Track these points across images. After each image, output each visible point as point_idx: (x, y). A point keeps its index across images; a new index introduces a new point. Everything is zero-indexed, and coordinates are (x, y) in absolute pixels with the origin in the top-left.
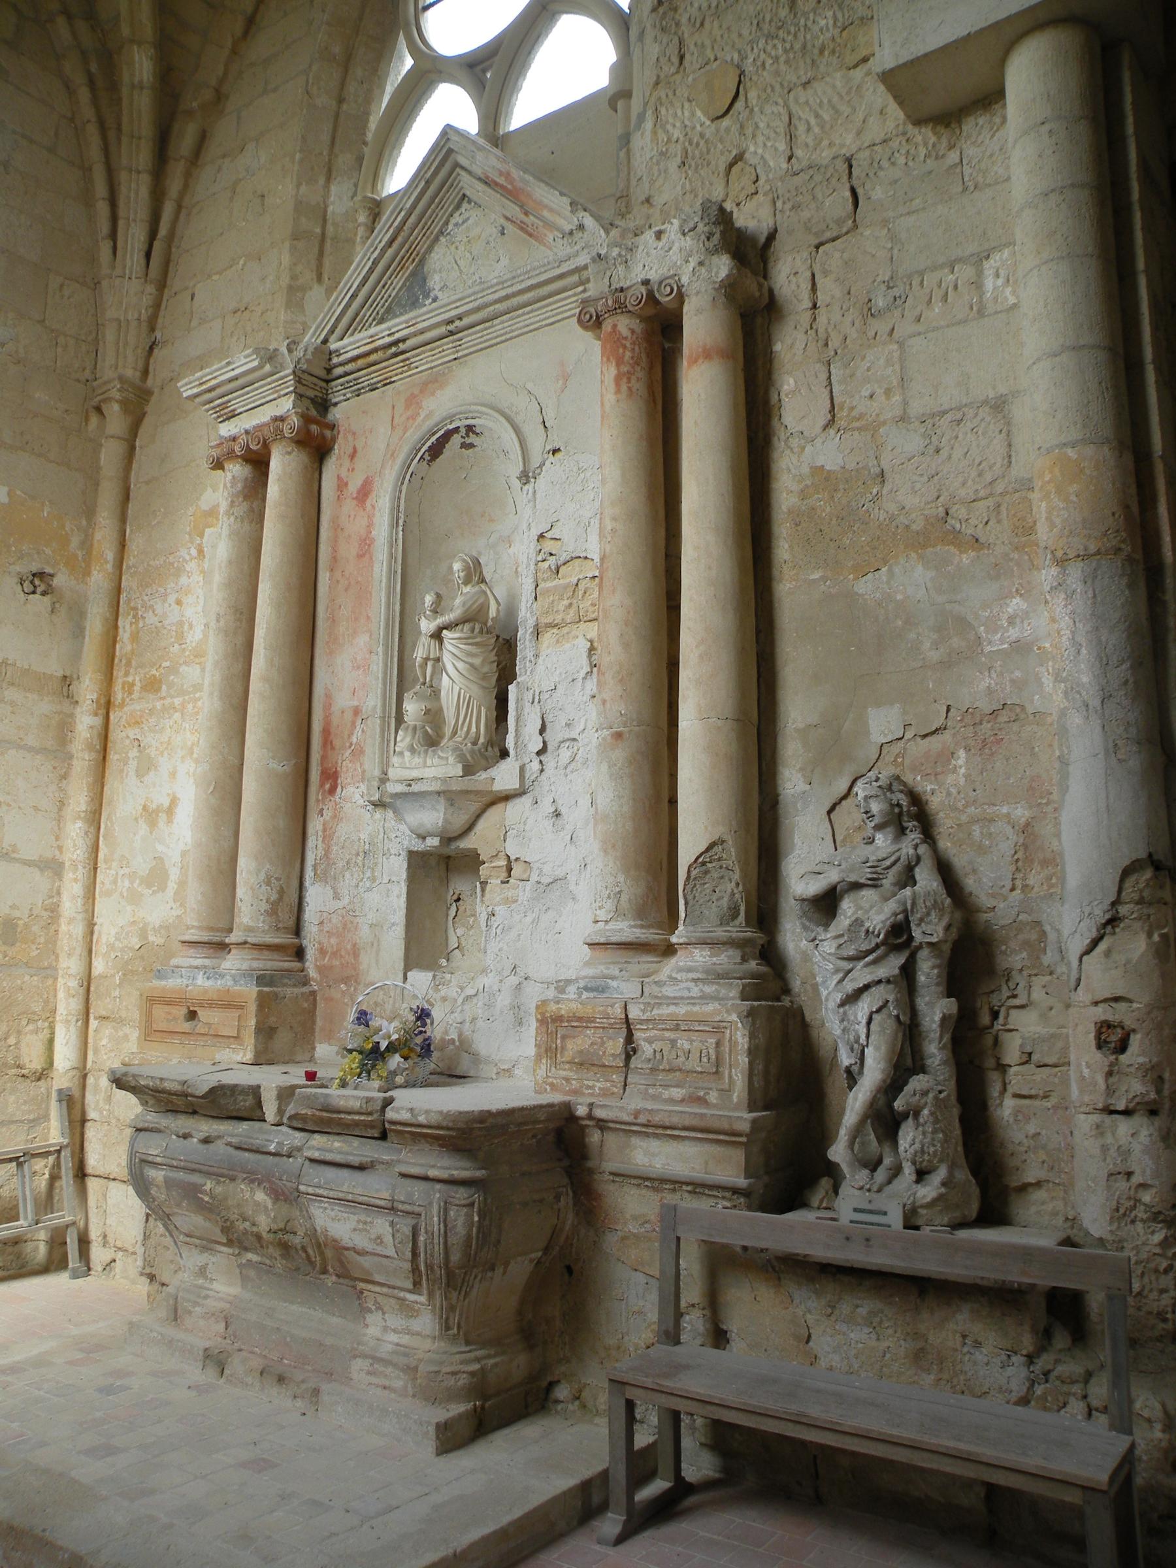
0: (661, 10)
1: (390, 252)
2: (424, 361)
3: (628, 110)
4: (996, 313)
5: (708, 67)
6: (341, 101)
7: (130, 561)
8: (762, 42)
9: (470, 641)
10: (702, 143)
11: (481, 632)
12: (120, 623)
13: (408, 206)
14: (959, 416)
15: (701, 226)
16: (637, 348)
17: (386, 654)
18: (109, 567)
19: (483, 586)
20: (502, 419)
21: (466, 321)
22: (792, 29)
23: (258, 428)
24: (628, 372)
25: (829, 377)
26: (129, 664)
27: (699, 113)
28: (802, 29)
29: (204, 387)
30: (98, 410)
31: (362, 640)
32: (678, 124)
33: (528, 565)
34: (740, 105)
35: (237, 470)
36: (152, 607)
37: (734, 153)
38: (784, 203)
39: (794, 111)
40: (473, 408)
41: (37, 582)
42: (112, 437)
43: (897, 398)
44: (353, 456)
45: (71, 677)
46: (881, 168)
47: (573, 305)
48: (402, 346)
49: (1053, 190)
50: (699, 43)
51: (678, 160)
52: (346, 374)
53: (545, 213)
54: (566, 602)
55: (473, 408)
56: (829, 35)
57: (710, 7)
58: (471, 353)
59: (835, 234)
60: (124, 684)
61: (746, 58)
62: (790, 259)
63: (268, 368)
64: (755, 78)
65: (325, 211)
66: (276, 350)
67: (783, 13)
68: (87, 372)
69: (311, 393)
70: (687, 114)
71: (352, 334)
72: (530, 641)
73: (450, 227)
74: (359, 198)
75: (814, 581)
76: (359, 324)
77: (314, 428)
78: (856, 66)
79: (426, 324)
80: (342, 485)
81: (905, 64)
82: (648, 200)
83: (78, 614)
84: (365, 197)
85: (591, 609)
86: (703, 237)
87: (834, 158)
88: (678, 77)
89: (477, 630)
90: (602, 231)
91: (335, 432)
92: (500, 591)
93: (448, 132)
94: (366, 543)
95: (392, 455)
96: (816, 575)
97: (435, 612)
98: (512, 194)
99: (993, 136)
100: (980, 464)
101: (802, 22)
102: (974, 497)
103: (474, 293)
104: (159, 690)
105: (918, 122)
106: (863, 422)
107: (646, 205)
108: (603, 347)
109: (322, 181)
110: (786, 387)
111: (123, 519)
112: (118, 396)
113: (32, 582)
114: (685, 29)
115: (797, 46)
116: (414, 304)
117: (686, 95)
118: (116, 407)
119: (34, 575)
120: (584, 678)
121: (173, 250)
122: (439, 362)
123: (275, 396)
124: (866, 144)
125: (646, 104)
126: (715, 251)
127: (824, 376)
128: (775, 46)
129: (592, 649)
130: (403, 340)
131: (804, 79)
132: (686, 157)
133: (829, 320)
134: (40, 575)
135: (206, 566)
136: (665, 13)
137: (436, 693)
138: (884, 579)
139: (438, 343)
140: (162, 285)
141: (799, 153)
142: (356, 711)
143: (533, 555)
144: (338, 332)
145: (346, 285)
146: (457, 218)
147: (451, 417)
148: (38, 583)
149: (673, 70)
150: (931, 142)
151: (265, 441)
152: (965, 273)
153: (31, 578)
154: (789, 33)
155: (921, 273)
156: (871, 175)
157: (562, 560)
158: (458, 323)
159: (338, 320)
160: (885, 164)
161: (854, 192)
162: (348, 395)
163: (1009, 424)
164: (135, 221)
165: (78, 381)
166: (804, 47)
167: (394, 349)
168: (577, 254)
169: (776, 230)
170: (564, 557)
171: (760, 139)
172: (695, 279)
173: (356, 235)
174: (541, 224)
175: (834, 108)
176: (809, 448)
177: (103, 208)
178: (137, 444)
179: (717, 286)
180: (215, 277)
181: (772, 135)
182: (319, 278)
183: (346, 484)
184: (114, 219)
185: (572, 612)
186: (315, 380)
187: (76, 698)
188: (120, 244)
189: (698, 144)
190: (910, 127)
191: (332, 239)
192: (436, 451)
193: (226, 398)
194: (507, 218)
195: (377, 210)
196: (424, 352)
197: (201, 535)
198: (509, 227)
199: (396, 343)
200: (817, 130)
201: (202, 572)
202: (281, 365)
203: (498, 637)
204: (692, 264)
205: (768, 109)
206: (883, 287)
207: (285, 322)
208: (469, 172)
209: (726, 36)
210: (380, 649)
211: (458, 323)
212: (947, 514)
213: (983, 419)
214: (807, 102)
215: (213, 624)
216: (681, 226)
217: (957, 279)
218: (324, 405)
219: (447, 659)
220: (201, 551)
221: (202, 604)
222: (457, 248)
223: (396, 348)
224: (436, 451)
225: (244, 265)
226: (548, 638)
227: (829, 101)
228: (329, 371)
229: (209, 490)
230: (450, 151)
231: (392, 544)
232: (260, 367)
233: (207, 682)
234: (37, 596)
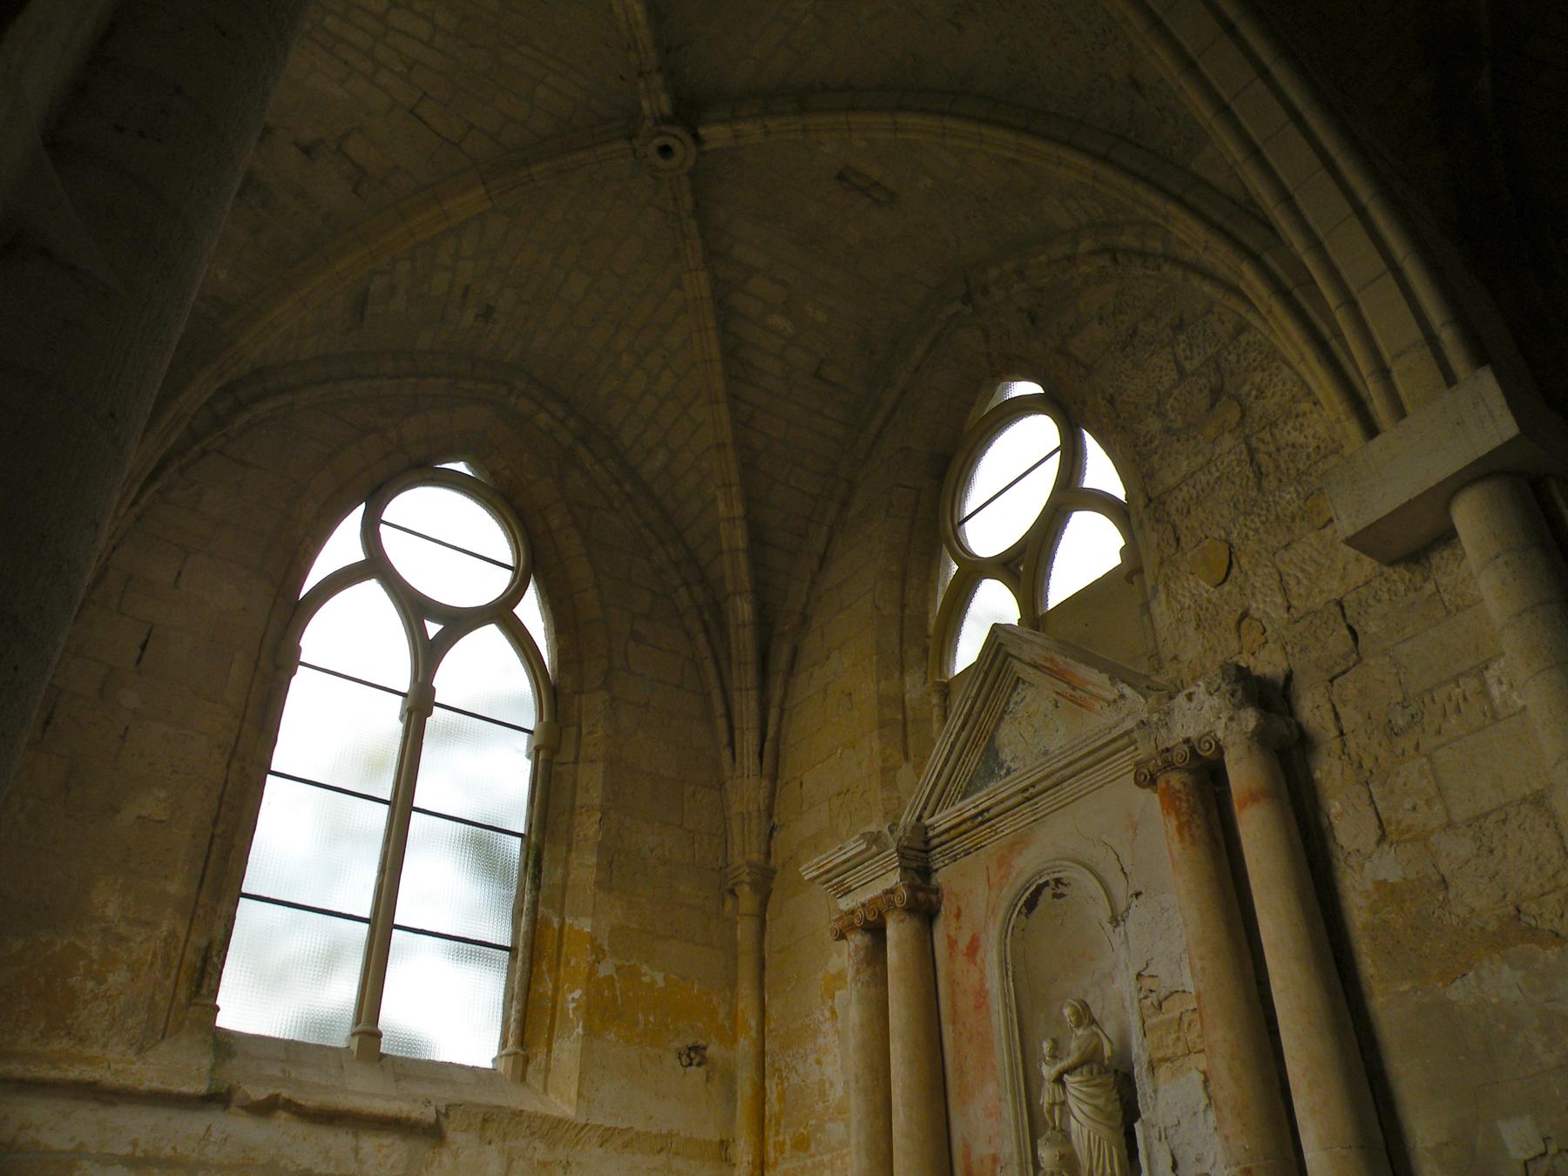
0: (1152, 505)
1: (964, 734)
2: (1007, 826)
3: (1143, 584)
4: (1510, 716)
5: (1201, 545)
6: (903, 607)
7: (771, 1025)
8: (1241, 519)
9: (1091, 1083)
10: (1211, 607)
11: (1100, 1072)
12: (767, 1084)
13: (973, 694)
14: (1502, 816)
15: (1223, 685)
16: (1191, 798)
17: (1014, 1101)
18: (753, 1033)
19: (1094, 1028)
20: (1087, 872)
21: (1039, 788)
22: (1264, 505)
23: (873, 901)
24: (1188, 821)
25: (1371, 796)
26: (778, 1123)
27: (1202, 583)
28: (1272, 504)
29: (822, 870)
30: (732, 892)
31: (991, 1088)
32: (1187, 594)
33: (1132, 1003)
34: (1235, 571)
35: (857, 940)
36: (794, 1067)
37: (1240, 611)
38: (1293, 648)
39: (1282, 569)
40: (1058, 863)
41: (692, 1055)
42: (745, 915)
43: (1438, 807)
44: (958, 915)
45: (728, 1141)
46: (1370, 606)
47: (1129, 762)
48: (987, 815)
49: (1524, 611)
50: (1189, 526)
51: (1194, 624)
52: (942, 844)
53: (1090, 687)
54: (1173, 1036)
55: (1058, 863)
56: (1295, 505)
57: (1191, 498)
58: (1049, 813)
59: (1344, 668)
60: (775, 1144)
61: (1231, 533)
62: (1309, 695)
63: (874, 848)
64: (1243, 548)
65: (903, 701)
66: (879, 832)
67: (1253, 493)
68: (720, 860)
69: (914, 864)
70: (1192, 585)
71: (940, 811)
72: (1147, 1077)
73: (1011, 705)
74: (929, 684)
75: (1405, 992)
76: (947, 798)
77: (921, 895)
78: (1324, 527)
79: (1004, 795)
80: (952, 944)
81: (1363, 530)
82: (1175, 658)
83: (730, 1080)
84: (936, 682)
85: (1198, 1041)
86: (1228, 695)
87: (1327, 603)
88: (1178, 556)
89: (1095, 1071)
90: (1140, 697)
91: (940, 895)
92: (1110, 1028)
93: (996, 629)
94: (981, 994)
95: (993, 912)
96: (1405, 987)
97: (1054, 1057)
98: (1059, 674)
99: (1459, 565)
100: (1537, 859)
101: (1271, 499)
102: (1540, 892)
103: (1042, 764)
104: (807, 1148)
105: (1392, 563)
106: (1413, 834)
107: (1175, 661)
108: (1162, 801)
109: (897, 675)
110: (1333, 810)
111: (761, 987)
112: (747, 879)
113: (689, 1056)
114: (1176, 518)
115: (1272, 518)
116: (991, 775)
117: (1188, 569)
118: (747, 888)
119: (690, 1049)
120: (1205, 1111)
121: (781, 746)
122: (1021, 824)
123: (883, 871)
124: (1352, 588)
125: (1156, 579)
126: (1240, 706)
127: (1365, 796)
128: (1252, 521)
129: (1206, 1081)
130: (987, 810)
131: (1284, 543)
132: (1200, 620)
133: (1357, 744)
134: (695, 1048)
135: (840, 1026)
136: (1155, 507)
137: (1067, 1136)
138: (1474, 983)
139: (1018, 809)
140: (774, 778)
141: (1295, 603)
142: (995, 1159)
143: (1135, 994)
144: (930, 808)
145: (931, 767)
146: (1015, 698)
147: (1040, 874)
148: (694, 1054)
149: (1173, 551)
150: (1407, 578)
151: (879, 912)
152: (1469, 685)
153: (687, 1051)
154: (1262, 509)
155: (1430, 691)
156: (1362, 613)
157: (1162, 996)
158: (1032, 790)
159: (928, 798)
160: (1371, 601)
161: (1351, 629)
162: (946, 862)
163: (1554, 817)
164: (748, 729)
165: (713, 870)
166: (1277, 517)
167: (980, 818)
168: (1123, 720)
169: (1291, 672)
170: (1164, 993)
171: (1259, 597)
172: (1228, 732)
173: (932, 714)
174: (1087, 696)
175: (1314, 561)
176: (1368, 864)
177: (721, 724)
178: (767, 918)
179: (1249, 735)
180: (819, 766)
181: (1269, 592)
182: (907, 758)
183: (956, 942)
184: (731, 729)
185: (1181, 1045)
186: (915, 853)
187: (733, 1161)
188: (738, 751)
189: (1207, 609)
190: (1385, 569)
191: (913, 722)
192: (1031, 904)
193: (841, 877)
194: (1058, 693)
195: (946, 691)
196: (1007, 818)
197: (832, 997)
198: (1062, 702)
199: (981, 813)
200: (1305, 582)
201: (837, 1032)
202: (885, 844)
203: (1116, 1071)
204: (1223, 721)
205: (1260, 571)
206: (1399, 708)
207: (882, 799)
208: (1020, 660)
209: (1210, 518)
210: (1009, 1097)
211: (1032, 790)
212: (1519, 911)
213: (1526, 816)
214: (1291, 560)
215: (853, 1084)
216: (1207, 688)
217: (1464, 690)
218: (926, 872)
219: (1071, 1102)
220: (833, 1012)
221: (839, 1063)
222: (1020, 723)
223: (981, 818)
224: (1031, 904)
225: (841, 754)
226: (1163, 1072)
227: (1310, 557)
228: (927, 842)
229: (835, 955)
230: (1001, 645)
231: (1005, 995)
232: (868, 849)
233: (853, 1141)
234: (694, 1068)
